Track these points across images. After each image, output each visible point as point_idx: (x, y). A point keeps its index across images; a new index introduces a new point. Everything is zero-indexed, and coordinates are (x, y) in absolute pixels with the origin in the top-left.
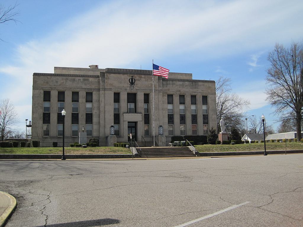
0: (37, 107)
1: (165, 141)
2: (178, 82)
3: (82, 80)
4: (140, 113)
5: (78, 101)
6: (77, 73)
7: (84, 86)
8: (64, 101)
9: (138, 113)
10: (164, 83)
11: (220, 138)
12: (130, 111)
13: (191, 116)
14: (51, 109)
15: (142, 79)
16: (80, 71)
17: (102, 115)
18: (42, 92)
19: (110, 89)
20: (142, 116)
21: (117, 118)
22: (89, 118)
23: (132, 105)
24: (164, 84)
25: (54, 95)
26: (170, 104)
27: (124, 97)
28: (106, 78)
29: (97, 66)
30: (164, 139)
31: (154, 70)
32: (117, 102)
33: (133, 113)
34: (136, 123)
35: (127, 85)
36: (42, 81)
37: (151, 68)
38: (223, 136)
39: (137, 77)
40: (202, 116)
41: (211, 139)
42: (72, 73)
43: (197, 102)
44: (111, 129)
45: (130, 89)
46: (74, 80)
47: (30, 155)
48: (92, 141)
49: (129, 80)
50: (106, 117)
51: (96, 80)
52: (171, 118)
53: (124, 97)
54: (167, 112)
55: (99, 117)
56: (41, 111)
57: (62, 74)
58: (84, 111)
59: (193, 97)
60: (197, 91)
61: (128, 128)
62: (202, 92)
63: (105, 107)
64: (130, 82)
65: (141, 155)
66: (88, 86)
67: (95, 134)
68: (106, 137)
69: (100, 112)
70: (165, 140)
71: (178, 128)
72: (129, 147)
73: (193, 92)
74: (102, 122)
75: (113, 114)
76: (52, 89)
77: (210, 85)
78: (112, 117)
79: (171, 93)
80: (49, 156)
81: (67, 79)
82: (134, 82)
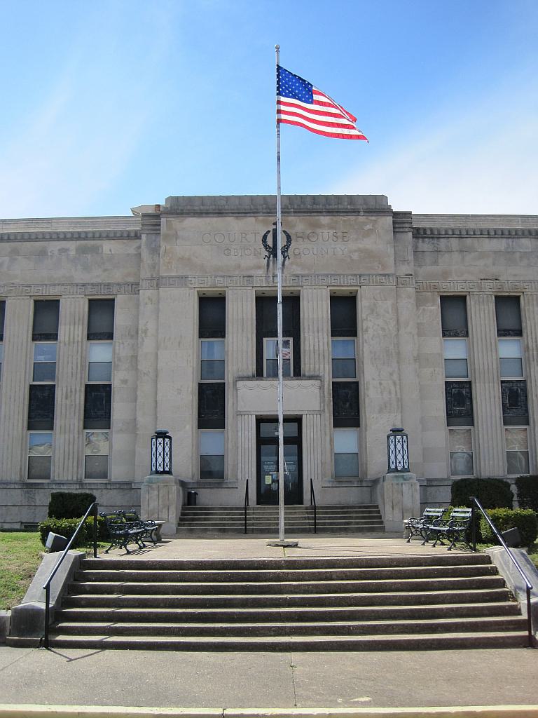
3: (72, 253)
7: (80, 276)
10: (425, 246)
15: (319, 231)
19: (182, 280)
20: (321, 388)
21: (211, 405)
46: (43, 253)
50: (159, 398)
52: (459, 401)
64: (266, 246)
66: (97, 275)
79: (454, 288)
81: (15, 252)
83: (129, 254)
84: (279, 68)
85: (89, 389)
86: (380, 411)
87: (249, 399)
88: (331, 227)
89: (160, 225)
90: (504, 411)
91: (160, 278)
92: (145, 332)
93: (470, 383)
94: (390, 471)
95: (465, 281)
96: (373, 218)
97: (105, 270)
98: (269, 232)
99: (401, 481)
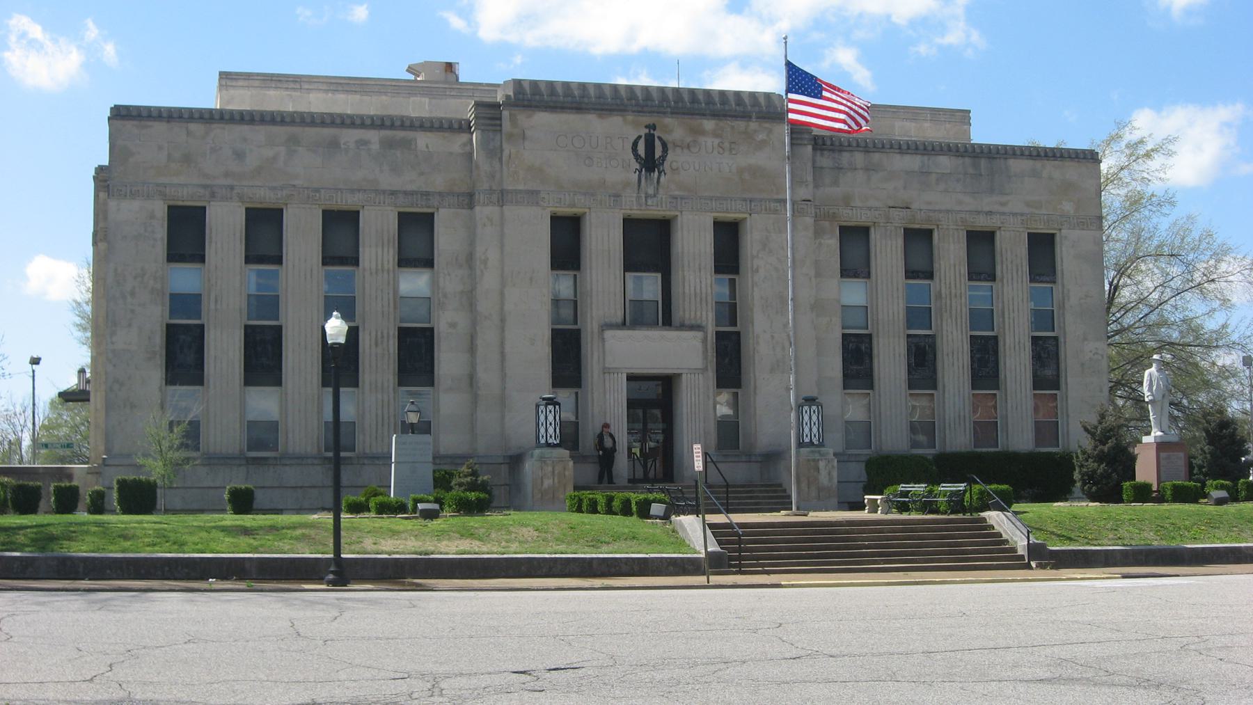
0: (133, 294)
1: (835, 481)
2: (898, 157)
3: (375, 147)
4: (692, 328)
5: (355, 261)
6: (344, 104)
7: (387, 181)
8: (278, 260)
9: (683, 327)
10: (825, 161)
11: (1146, 471)
12: (637, 317)
13: (967, 347)
14: (212, 306)
15: (702, 139)
16: (358, 97)
17: (487, 337)
18: (160, 210)
19: (532, 196)
20: (705, 341)
21: (568, 356)
22: (416, 353)
23: (649, 286)
24: (822, 168)
25: (225, 227)
26: (856, 276)
27: (603, 241)
28: (511, 136)
29: (450, 67)
30: (828, 473)
31: (791, 96)
32: (568, 269)
33: (653, 324)
34: (668, 383)
35: (624, 171)
36: (160, 148)
37: (772, 83)
38: (1163, 455)
39: (674, 130)
40: (1028, 345)
41: (1094, 471)
42: (317, 103)
43: (998, 268)
44: (542, 418)
45: (638, 198)
46: (334, 145)
47: (146, 559)
48: (460, 485)
49: (635, 144)
50: (507, 349)
51: (456, 143)
52: (857, 358)
53: (603, 241)
54: (837, 322)
55: (472, 349)
56: (155, 317)
57: (256, 117)
58: (392, 317)
59: (981, 242)
60: (996, 208)
61: (628, 408)
62: (1026, 210)
63: (498, 297)
64: (637, 156)
65: (740, 558)
66: (409, 180)
67: (451, 440)
68: (511, 457)
69: (474, 324)
70: (835, 474)
71: (892, 409)
72: (666, 517)
73: (978, 212)
74: (487, 377)
75: (547, 335)
76: (213, 195)
77: (1071, 171)
78: (543, 350)
79: (857, 217)
80: (247, 565)
81: (293, 141)
82: (663, 157)
83: (451, 153)
84: (790, 66)
85: (404, 333)
86: (772, 370)
87: (623, 353)
88: (716, 135)
89: (500, 119)
90: (909, 373)
91: (503, 192)
92: (485, 262)
93: (870, 336)
94: (539, 445)
95: (870, 209)
96: (767, 125)
97: (422, 174)
98: (640, 137)
99: (817, 456)
